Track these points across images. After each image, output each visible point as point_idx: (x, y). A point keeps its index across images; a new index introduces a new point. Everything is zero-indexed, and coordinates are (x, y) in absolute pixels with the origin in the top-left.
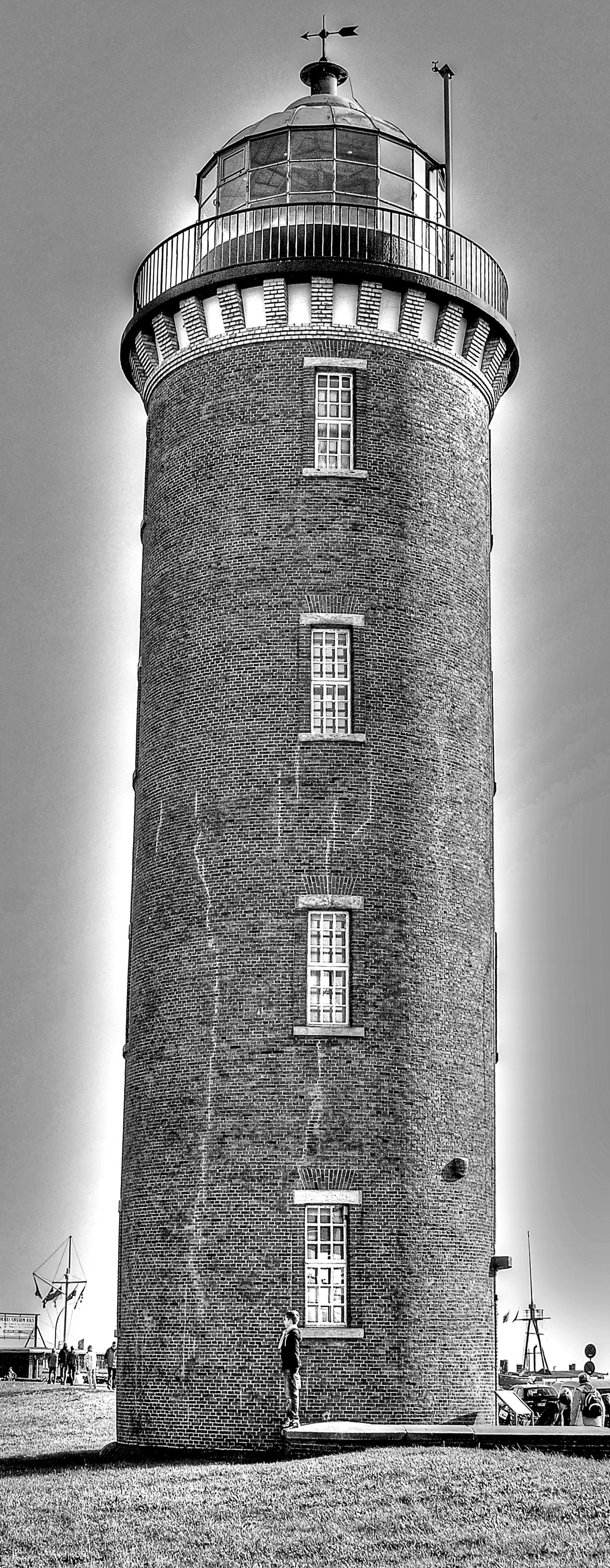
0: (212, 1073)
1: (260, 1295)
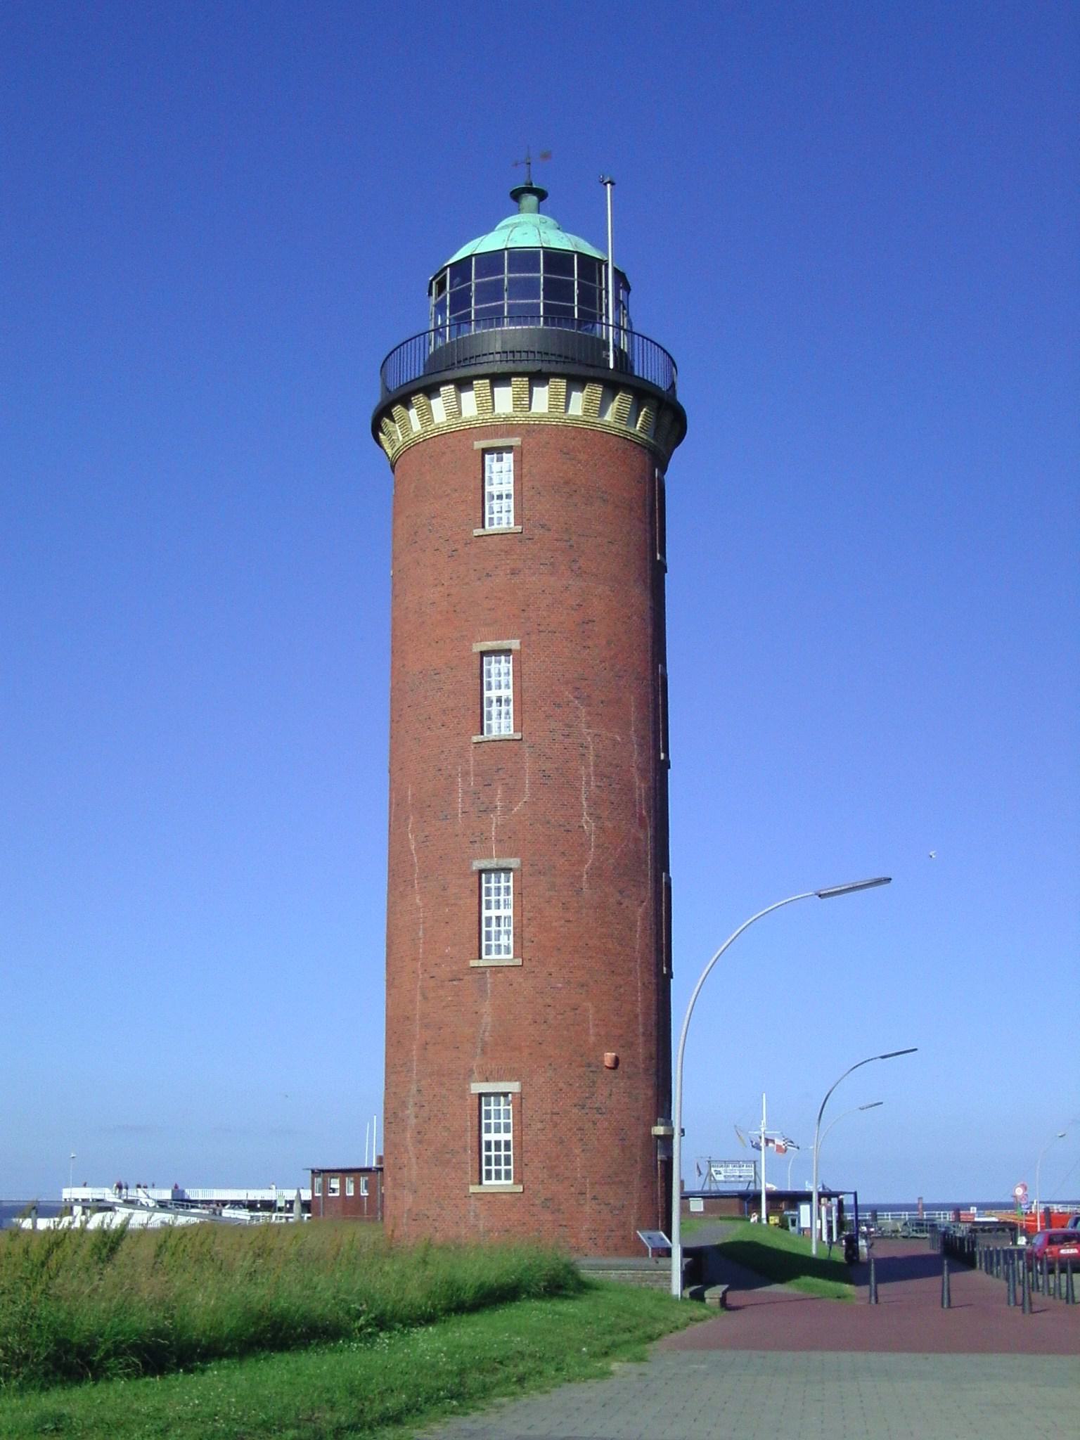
0: (419, 997)
1: (449, 1161)
